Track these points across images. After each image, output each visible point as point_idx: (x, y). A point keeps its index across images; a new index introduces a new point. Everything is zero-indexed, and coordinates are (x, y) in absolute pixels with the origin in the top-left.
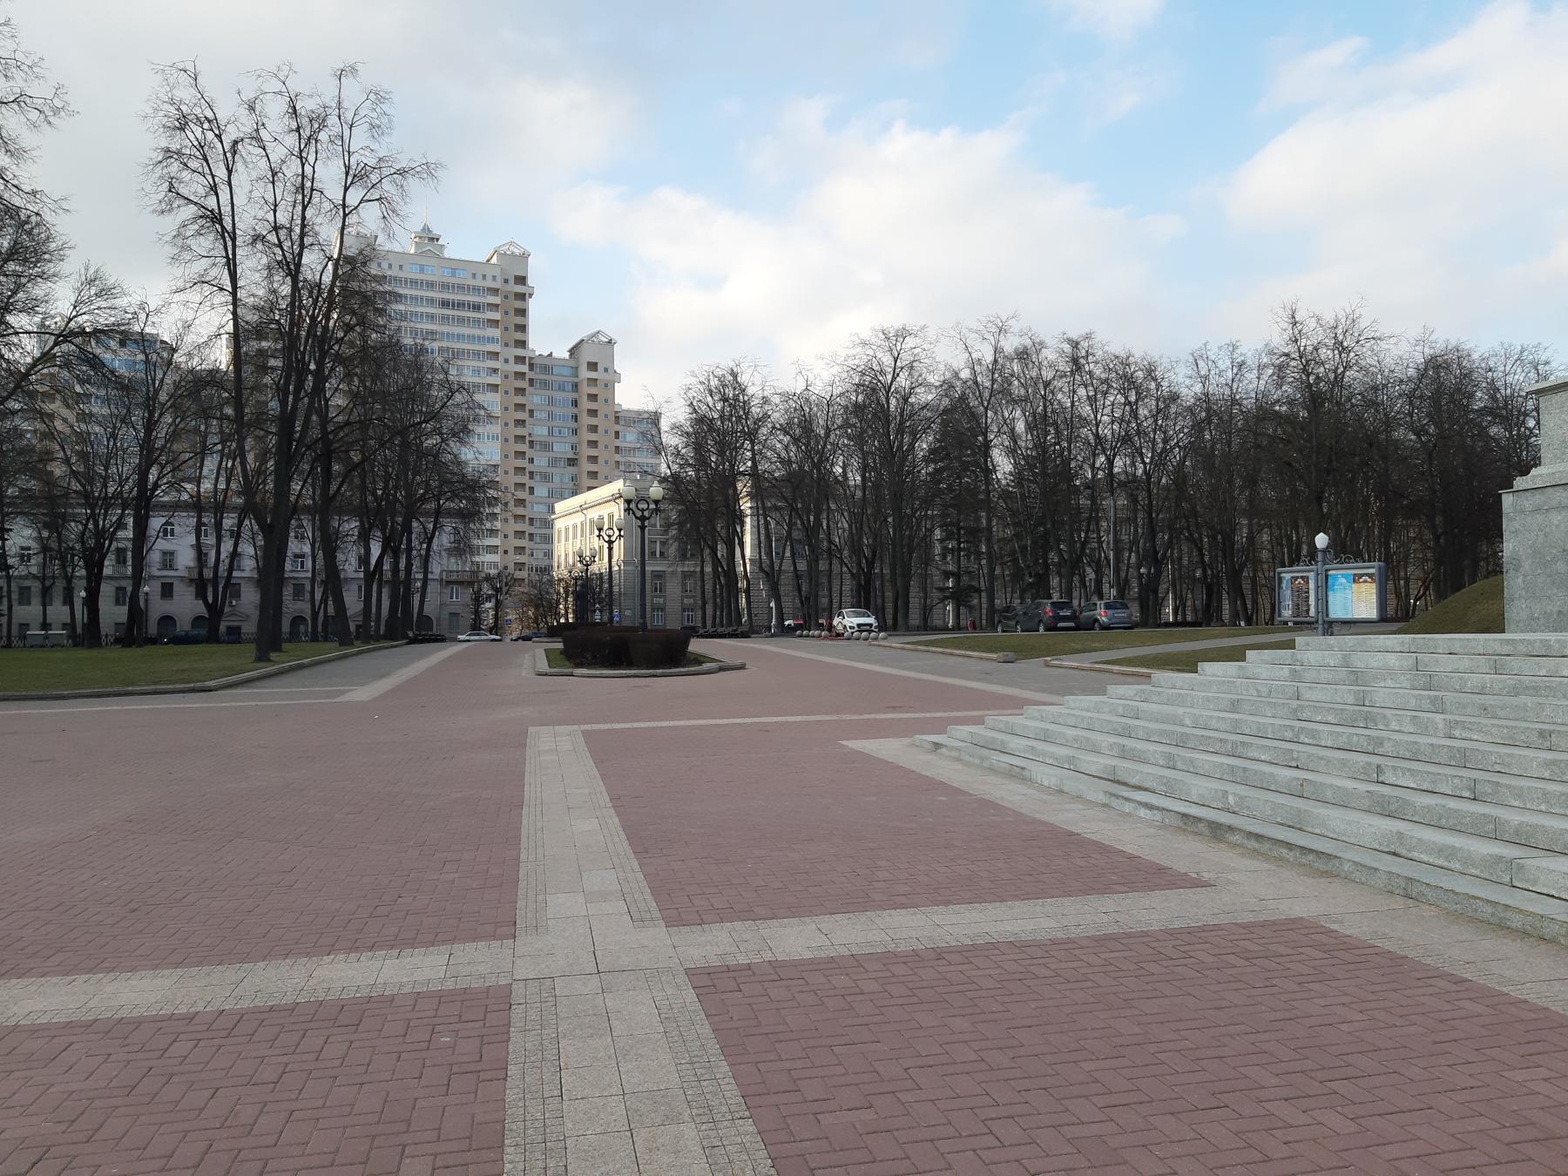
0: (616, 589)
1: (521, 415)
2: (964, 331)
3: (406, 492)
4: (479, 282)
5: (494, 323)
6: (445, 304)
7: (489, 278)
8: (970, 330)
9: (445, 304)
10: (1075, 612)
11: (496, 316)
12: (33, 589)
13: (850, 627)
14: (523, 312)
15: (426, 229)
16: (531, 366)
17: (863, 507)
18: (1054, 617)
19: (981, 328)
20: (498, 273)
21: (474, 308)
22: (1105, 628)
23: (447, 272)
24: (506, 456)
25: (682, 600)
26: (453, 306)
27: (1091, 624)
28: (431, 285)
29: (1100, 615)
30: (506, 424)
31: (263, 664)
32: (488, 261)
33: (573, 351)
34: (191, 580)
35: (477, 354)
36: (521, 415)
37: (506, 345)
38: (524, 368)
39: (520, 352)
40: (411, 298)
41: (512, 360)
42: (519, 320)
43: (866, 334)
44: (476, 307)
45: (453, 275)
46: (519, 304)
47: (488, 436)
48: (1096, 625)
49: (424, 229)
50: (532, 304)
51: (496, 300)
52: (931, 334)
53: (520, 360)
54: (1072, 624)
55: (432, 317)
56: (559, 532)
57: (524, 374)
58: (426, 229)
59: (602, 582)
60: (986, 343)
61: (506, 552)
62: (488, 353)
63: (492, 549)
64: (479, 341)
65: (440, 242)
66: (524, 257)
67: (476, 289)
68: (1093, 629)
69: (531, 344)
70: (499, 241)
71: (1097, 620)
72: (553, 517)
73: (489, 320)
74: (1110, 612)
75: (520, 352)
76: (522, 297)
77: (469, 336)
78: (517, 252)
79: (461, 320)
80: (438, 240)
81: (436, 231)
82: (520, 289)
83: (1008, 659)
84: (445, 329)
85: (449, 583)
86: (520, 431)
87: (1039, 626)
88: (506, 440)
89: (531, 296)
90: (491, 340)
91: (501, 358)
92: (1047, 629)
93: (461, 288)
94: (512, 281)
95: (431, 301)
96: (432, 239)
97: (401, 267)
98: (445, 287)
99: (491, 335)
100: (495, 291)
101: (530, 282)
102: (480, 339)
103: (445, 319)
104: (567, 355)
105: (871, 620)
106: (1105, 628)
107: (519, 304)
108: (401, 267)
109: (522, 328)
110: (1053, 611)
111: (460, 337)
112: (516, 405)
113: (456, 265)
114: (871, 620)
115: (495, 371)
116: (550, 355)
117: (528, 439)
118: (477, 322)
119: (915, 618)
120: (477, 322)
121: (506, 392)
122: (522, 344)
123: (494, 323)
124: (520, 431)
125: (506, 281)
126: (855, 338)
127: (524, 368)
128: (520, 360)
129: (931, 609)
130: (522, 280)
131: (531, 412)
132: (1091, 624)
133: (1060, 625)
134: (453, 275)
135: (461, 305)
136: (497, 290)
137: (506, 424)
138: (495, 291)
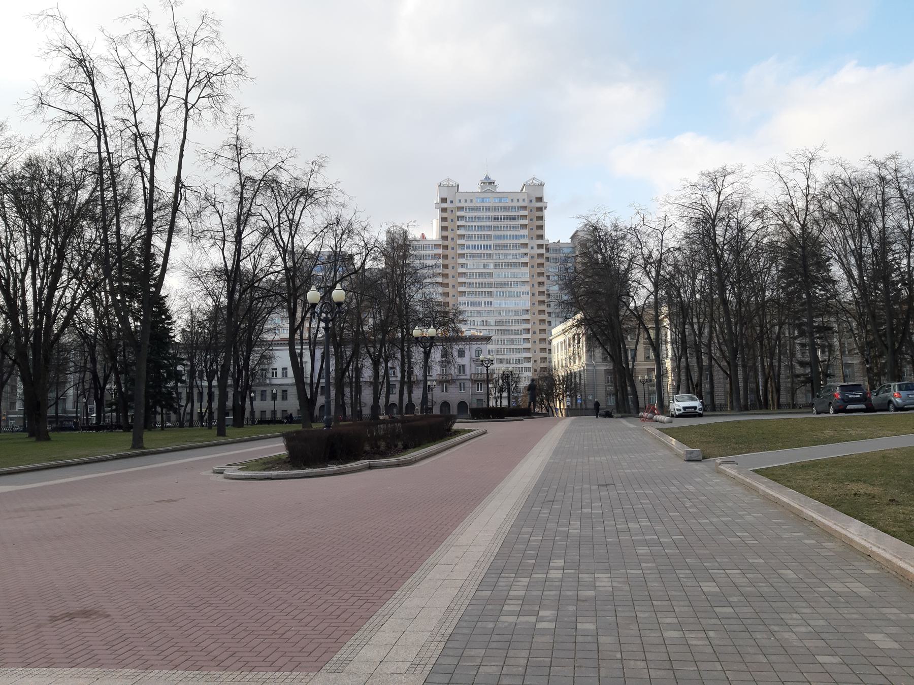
0: (582, 382)
1: (541, 279)
2: (778, 164)
3: (681, 336)
4: (515, 204)
5: (524, 227)
6: (496, 219)
7: (521, 201)
8: (782, 163)
9: (496, 219)
10: (865, 394)
11: (525, 222)
12: (267, 392)
13: (678, 410)
14: (541, 218)
15: (487, 178)
16: (547, 250)
17: (231, 274)
18: (842, 399)
19: (791, 160)
20: (526, 197)
21: (513, 219)
22: (898, 408)
23: (497, 200)
24: (534, 304)
25: (606, 388)
26: (501, 219)
27: (886, 405)
28: (488, 209)
29: (894, 397)
30: (533, 285)
31: (221, 438)
32: (522, 190)
33: (573, 238)
34: (371, 383)
35: (515, 246)
36: (541, 279)
37: (532, 238)
38: (543, 251)
39: (540, 242)
40: (486, 217)
41: (535, 247)
42: (539, 223)
43: (695, 179)
44: (514, 219)
45: (501, 201)
46: (539, 214)
47: (523, 293)
48: (891, 406)
49: (486, 178)
50: (547, 214)
51: (525, 213)
52: (747, 170)
53: (540, 246)
54: (863, 406)
55: (489, 227)
56: (554, 347)
57: (543, 254)
58: (487, 178)
59: (571, 378)
60: (798, 173)
61: (535, 361)
62: (521, 244)
63: (527, 360)
64: (504, 238)
65: (495, 184)
66: (542, 185)
67: (514, 208)
68: (888, 410)
69: (547, 237)
70: (525, 178)
71: (890, 402)
72: (550, 338)
73: (521, 225)
74: (903, 394)
75: (540, 242)
76: (540, 209)
77: (510, 236)
78: (537, 183)
79: (506, 227)
80: (494, 183)
81: (492, 178)
82: (539, 205)
83: (694, 456)
84: (497, 233)
85: (476, 381)
86: (542, 289)
87: (829, 408)
88: (533, 295)
89: (546, 208)
90: (523, 237)
91: (529, 246)
92: (836, 412)
93: (505, 208)
94: (534, 201)
95: (488, 218)
96: (490, 183)
97: (471, 200)
98: (496, 209)
99: (523, 234)
100: (524, 208)
101: (545, 200)
102: (517, 237)
103: (496, 227)
104: (569, 241)
105: (697, 404)
106: (898, 408)
107: (539, 214)
108: (471, 200)
109: (541, 228)
110: (842, 394)
111: (506, 237)
112: (538, 273)
113: (502, 196)
114: (697, 404)
115: (526, 254)
116: (559, 242)
117: (546, 293)
118: (514, 227)
119: (784, 398)
120: (514, 227)
121: (533, 266)
122: (541, 237)
123: (524, 227)
124: (542, 289)
125: (531, 201)
126: (684, 182)
127: (543, 251)
128: (540, 246)
129: (796, 391)
130: (540, 199)
131: (548, 277)
132: (886, 405)
133: (849, 407)
134: (501, 201)
135: (505, 218)
136: (526, 207)
137: (533, 285)
138: (524, 208)
